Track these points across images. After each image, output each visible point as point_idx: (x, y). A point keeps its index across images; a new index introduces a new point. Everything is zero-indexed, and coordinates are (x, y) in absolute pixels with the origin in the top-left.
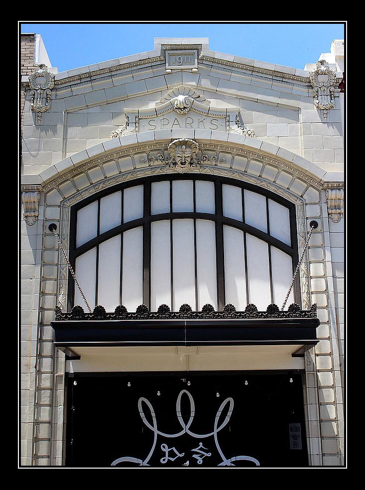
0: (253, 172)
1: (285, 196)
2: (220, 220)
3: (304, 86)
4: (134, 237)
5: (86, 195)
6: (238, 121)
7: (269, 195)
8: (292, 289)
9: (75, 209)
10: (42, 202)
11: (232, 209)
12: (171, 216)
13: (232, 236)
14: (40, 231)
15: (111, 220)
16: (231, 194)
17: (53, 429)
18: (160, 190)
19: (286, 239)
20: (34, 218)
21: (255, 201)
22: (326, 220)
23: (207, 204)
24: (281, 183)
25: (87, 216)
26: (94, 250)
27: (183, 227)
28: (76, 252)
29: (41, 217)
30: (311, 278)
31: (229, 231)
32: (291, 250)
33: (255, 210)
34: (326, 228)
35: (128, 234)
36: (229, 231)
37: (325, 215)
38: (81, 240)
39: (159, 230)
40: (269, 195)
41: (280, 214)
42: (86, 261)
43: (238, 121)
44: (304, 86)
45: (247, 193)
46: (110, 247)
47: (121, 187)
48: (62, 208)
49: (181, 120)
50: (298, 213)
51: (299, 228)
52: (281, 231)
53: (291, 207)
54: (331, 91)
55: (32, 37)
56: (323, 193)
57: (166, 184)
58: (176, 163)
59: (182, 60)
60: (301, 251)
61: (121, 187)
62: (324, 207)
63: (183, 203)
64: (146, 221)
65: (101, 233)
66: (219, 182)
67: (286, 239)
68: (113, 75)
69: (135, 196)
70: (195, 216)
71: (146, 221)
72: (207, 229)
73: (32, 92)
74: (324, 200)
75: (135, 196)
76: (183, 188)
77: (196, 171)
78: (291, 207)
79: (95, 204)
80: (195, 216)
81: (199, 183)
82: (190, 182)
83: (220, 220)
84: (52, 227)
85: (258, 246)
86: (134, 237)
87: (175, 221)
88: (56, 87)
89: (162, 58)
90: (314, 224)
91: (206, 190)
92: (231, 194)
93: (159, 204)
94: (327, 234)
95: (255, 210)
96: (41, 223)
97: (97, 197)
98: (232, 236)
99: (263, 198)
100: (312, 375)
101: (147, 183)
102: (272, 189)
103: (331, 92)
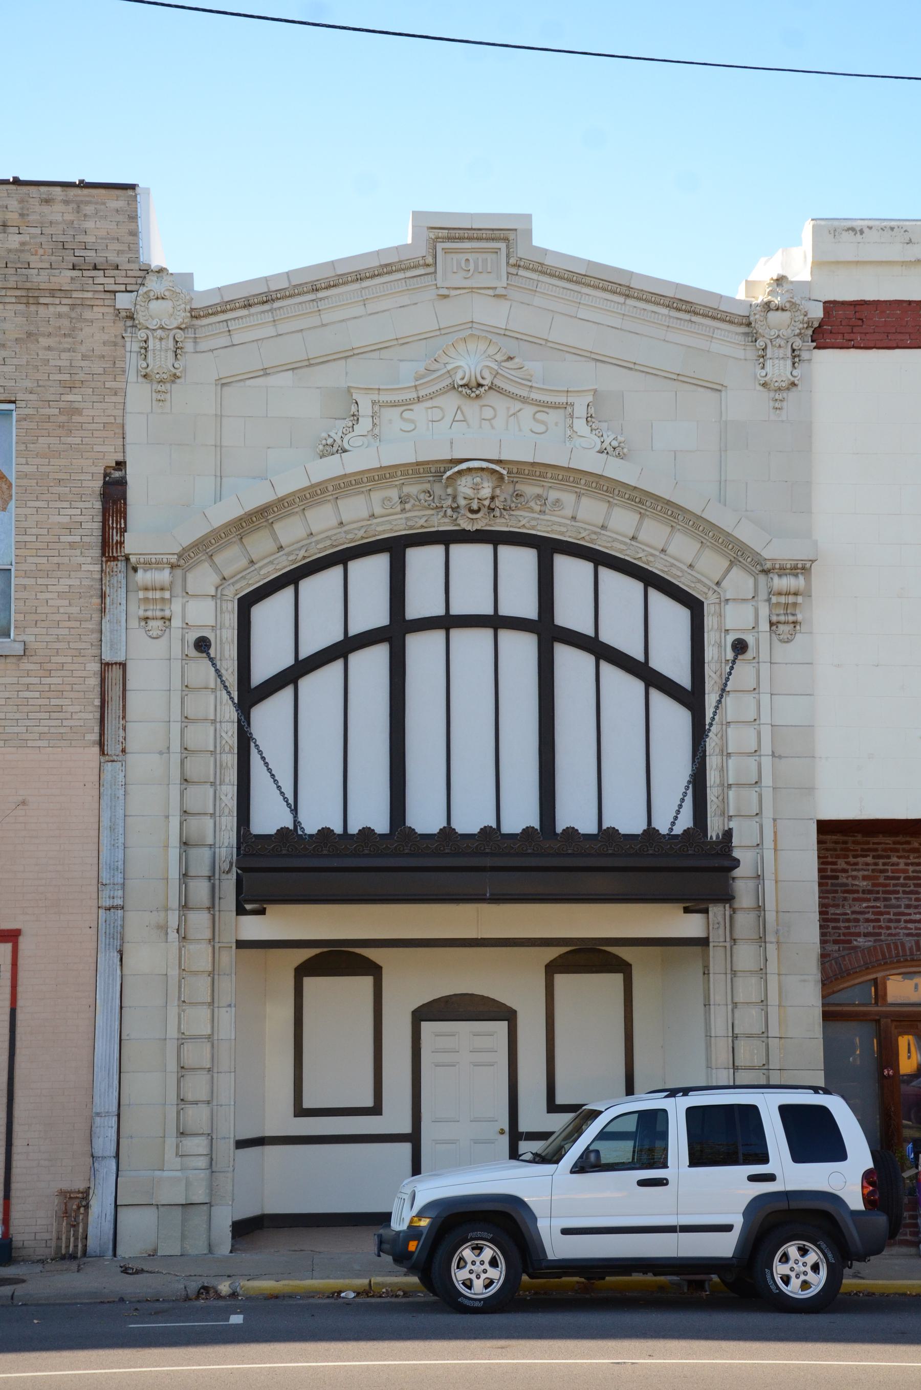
0: (618, 529)
1: (684, 583)
2: (548, 632)
3: (737, 334)
4: (371, 664)
5: (270, 573)
6: (591, 416)
7: (651, 580)
8: (708, 721)
9: (246, 604)
10: (178, 589)
11: (572, 613)
12: (448, 622)
13: (572, 664)
14: (177, 651)
15: (321, 633)
16: (571, 574)
17: (215, 1050)
18: (423, 562)
19: (682, 676)
20: (160, 623)
21: (621, 591)
22: (764, 637)
23: (521, 601)
24: (677, 554)
25: (271, 615)
26: (288, 691)
27: (472, 644)
28: (249, 696)
29: (176, 623)
30: (729, 755)
31: (564, 654)
32: (691, 698)
33: (622, 610)
34: (764, 655)
35: (357, 659)
36: (564, 654)
37: (764, 626)
38: (263, 669)
39: (423, 649)
40: (651, 580)
41: (671, 618)
42: (270, 717)
43: (591, 416)
44: (737, 334)
45: (606, 574)
46: (321, 686)
47: (342, 558)
48: (219, 601)
49: (471, 409)
50: (709, 622)
51: (710, 653)
52: (673, 662)
53: (695, 606)
54: (794, 347)
55: (130, 192)
56: (762, 578)
57: (437, 551)
58: (458, 507)
59: (472, 267)
60: (711, 700)
61: (342, 558)
62: (764, 611)
63: (471, 599)
64: (396, 632)
65: (604, 827)
66: (547, 549)
67: (682, 676)
68: (321, 299)
69: (372, 573)
70: (496, 622)
71: (396, 632)
72: (521, 649)
73: (142, 334)
74: (763, 595)
75: (372, 573)
76: (471, 559)
77: (500, 526)
78: (695, 606)
79: (289, 592)
80: (496, 622)
81: (505, 551)
82: (488, 549)
83: (548, 632)
84: (202, 645)
85: (623, 688)
86: (371, 664)
87: (454, 633)
88: (197, 322)
89: (430, 260)
90: (740, 647)
91: (520, 563)
92: (571, 574)
93: (423, 601)
94: (765, 668)
95: (622, 610)
96: (176, 634)
97: (291, 579)
98: (572, 664)
99: (638, 586)
100: (723, 949)
101: (396, 549)
102: (657, 567)
103: (793, 350)
